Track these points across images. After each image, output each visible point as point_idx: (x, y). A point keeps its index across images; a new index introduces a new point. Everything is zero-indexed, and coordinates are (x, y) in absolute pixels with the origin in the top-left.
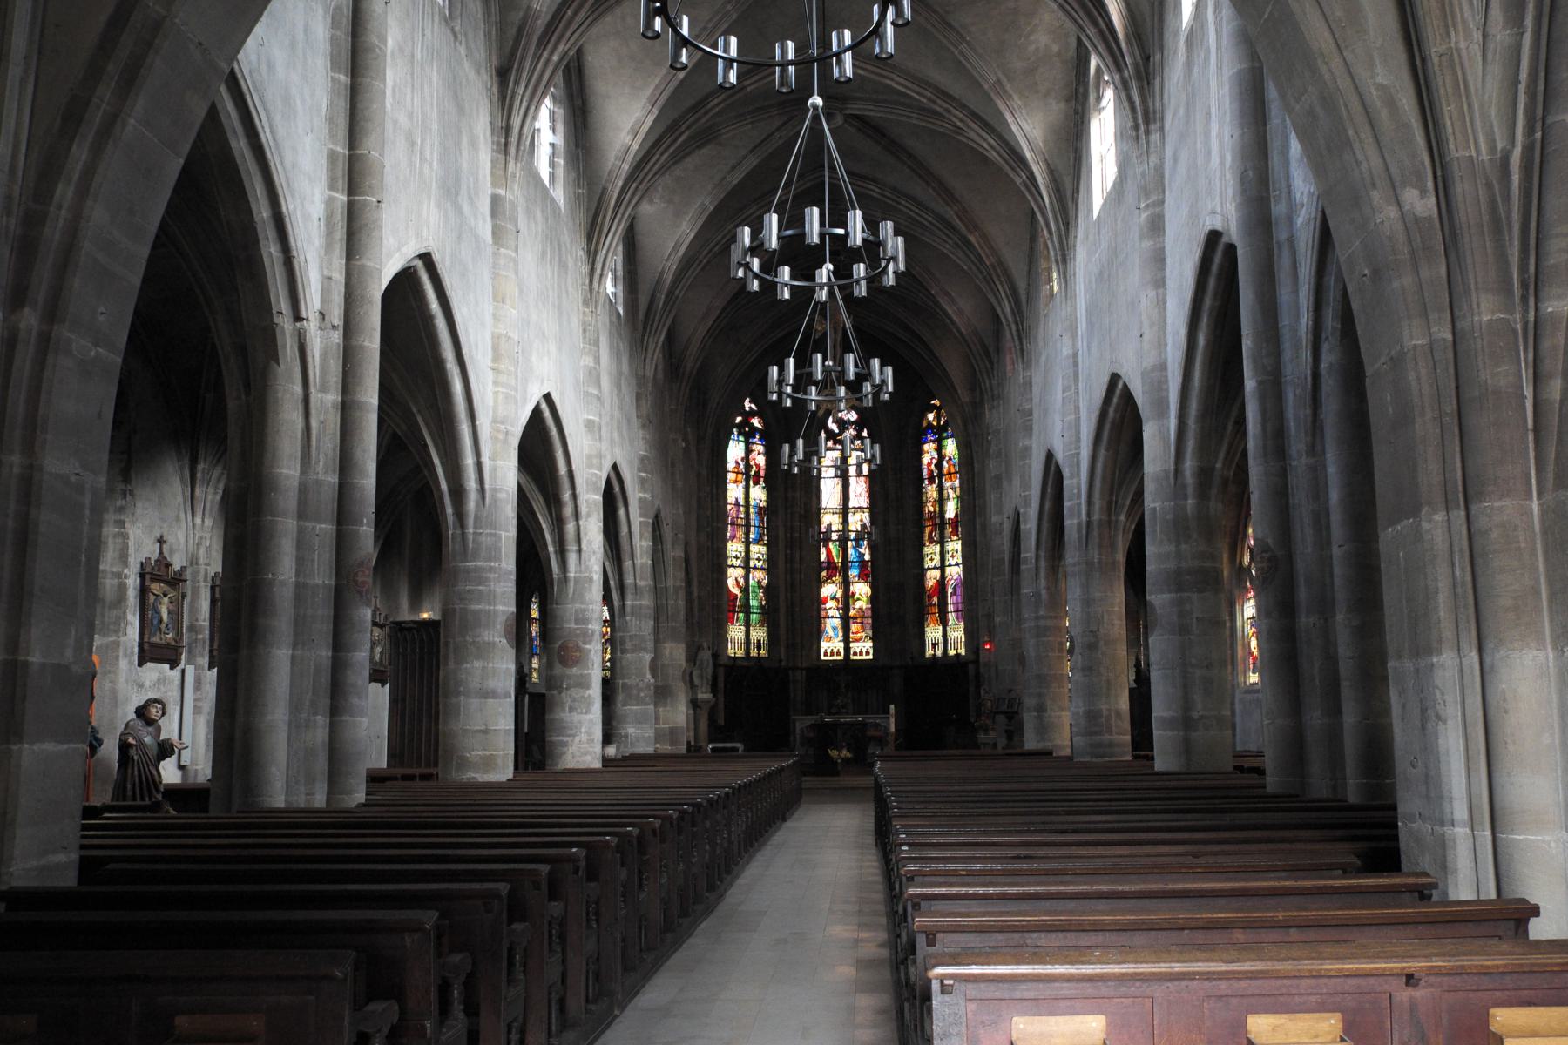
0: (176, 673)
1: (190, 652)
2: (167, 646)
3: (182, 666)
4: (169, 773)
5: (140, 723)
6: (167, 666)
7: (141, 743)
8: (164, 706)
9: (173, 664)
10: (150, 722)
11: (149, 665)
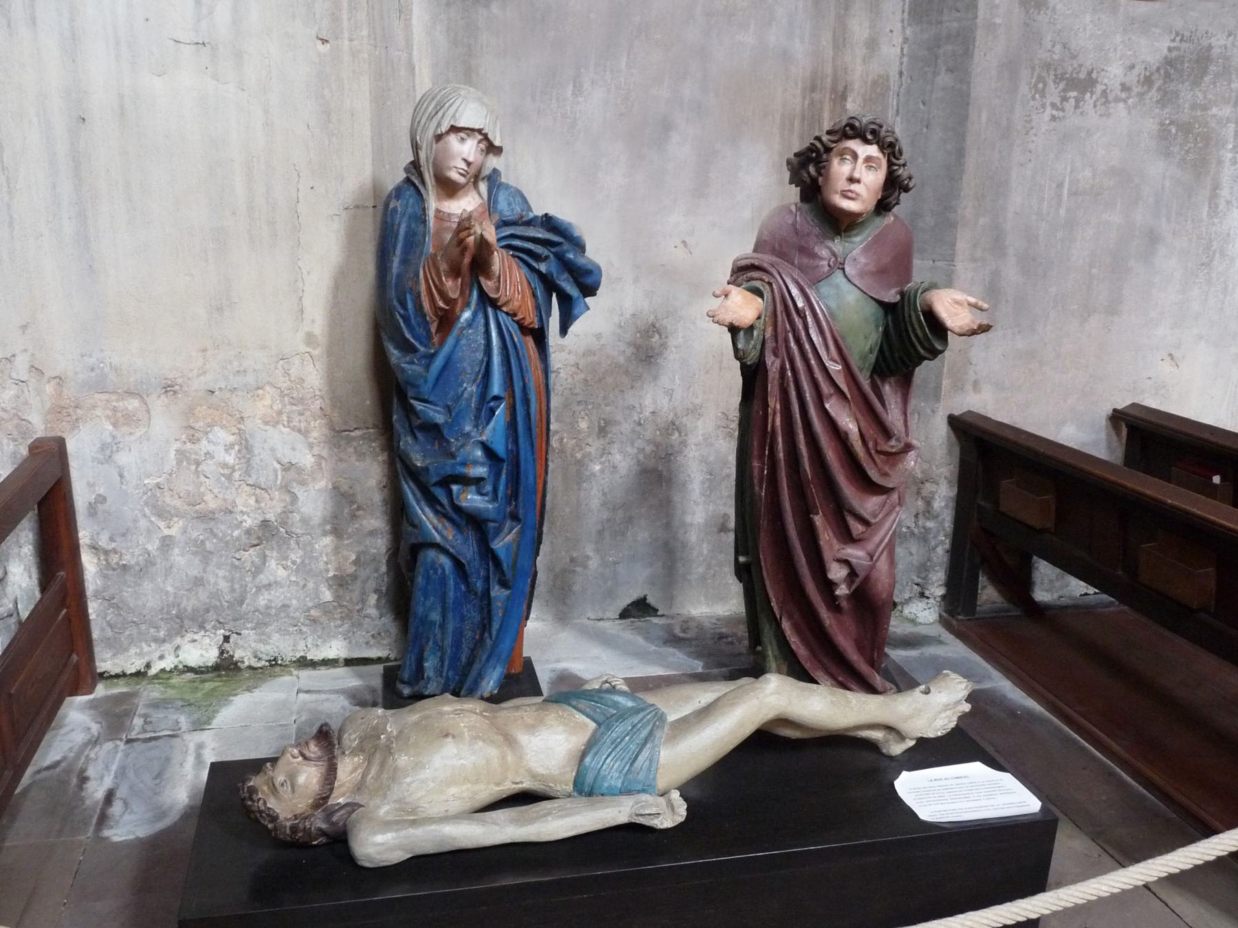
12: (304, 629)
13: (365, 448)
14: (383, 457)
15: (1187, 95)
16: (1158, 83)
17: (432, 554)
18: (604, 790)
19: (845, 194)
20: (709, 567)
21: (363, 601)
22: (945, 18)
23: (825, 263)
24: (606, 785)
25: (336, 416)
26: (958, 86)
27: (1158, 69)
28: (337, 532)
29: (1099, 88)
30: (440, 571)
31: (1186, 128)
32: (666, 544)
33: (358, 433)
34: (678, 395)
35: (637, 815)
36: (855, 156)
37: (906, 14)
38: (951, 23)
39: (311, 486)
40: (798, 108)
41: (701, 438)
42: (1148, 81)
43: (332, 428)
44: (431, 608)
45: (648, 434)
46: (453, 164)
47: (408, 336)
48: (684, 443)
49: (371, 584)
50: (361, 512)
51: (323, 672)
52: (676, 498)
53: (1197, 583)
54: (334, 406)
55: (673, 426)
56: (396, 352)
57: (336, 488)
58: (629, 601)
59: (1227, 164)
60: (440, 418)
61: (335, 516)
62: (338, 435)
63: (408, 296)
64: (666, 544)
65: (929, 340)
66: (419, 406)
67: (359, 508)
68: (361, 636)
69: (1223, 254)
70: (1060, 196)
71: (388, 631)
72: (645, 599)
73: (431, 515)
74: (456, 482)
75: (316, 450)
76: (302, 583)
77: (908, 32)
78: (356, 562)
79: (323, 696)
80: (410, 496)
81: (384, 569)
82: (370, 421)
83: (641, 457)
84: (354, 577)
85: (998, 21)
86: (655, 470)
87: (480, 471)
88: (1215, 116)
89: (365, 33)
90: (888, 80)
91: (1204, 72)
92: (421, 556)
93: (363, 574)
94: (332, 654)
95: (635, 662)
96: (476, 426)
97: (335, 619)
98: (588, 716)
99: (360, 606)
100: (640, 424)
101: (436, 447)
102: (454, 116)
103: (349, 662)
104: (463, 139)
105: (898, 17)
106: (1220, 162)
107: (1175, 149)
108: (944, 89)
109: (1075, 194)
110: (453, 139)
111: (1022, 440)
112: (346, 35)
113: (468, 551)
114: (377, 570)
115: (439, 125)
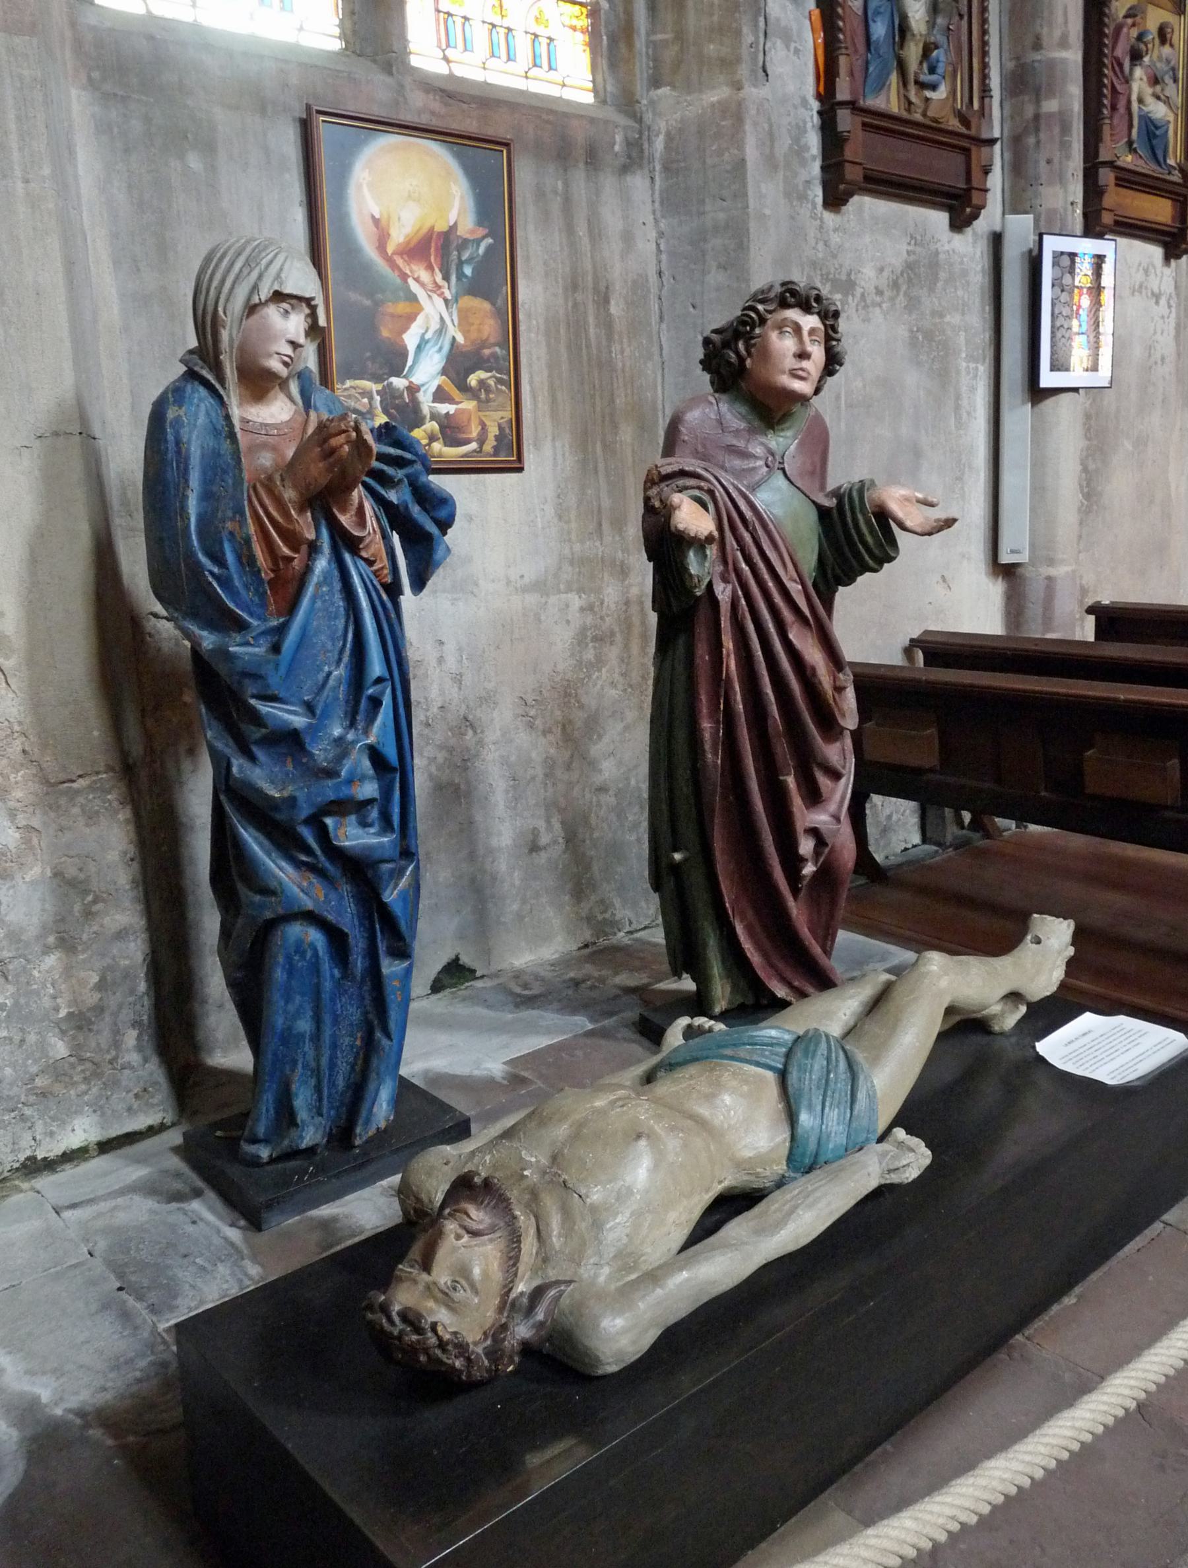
0: (966, 250)
1: (1018, 168)
2: (929, 134)
3: (991, 216)
4: (876, 622)
5: (729, 413)
6: (939, 219)
7: (736, 521)
8: (830, 317)
9: (961, 207)
10: (770, 408)
11: (864, 205)
12: (28, 1112)
13: (97, 805)
14: (125, 814)
15: (929, 303)
16: (904, 288)
17: (296, 930)
18: (830, 1156)
19: (794, 374)
20: (524, 902)
21: (116, 1044)
22: (708, 208)
23: (760, 463)
24: (831, 1146)
25: (48, 761)
26: (735, 285)
27: (902, 274)
28: (67, 944)
29: (859, 291)
30: (309, 954)
31: (929, 336)
32: (473, 880)
33: (81, 783)
34: (468, 680)
35: (889, 1171)
36: (797, 329)
37: (657, 205)
38: (715, 213)
39: (18, 877)
40: (561, 311)
41: (498, 733)
42: (895, 285)
43: (46, 782)
44: (297, 1015)
45: (438, 738)
46: (275, 348)
47: (231, 605)
48: (481, 743)
49: (126, 1015)
50: (99, 906)
51: (68, 1172)
52: (478, 818)
53: (1161, 779)
54: (44, 746)
55: (468, 723)
56: (205, 633)
57: (58, 874)
58: (439, 967)
59: (963, 373)
60: (299, 721)
61: (61, 919)
62: (54, 790)
63: (227, 547)
64: (473, 880)
65: (881, 545)
66: (264, 708)
67: (95, 902)
68: (120, 1100)
69: (970, 467)
70: (838, 408)
71: (156, 1083)
72: (457, 959)
73: (289, 869)
74: (329, 813)
75: (22, 820)
76: (17, 1038)
77: (663, 225)
78: (101, 986)
79: (104, 1206)
80: (256, 848)
81: (142, 986)
82: (101, 761)
83: (433, 769)
84: (99, 1009)
85: (767, 212)
86: (451, 784)
87: (369, 789)
88: (949, 323)
89: (47, 171)
90: (647, 280)
91: (936, 279)
92: (277, 938)
93: (113, 1001)
94: (74, 1140)
95: (504, 1038)
96: (352, 724)
97: (74, 1084)
98: (758, 1064)
99: (113, 1053)
100: (428, 725)
101: (290, 767)
102: (278, 277)
103: (105, 1147)
104: (287, 312)
105: (648, 207)
106: (958, 372)
107: (923, 358)
108: (718, 289)
109: (851, 406)
110: (272, 313)
111: (882, 671)
112: (18, 173)
113: (344, 910)
114: (132, 991)
115: (255, 288)
